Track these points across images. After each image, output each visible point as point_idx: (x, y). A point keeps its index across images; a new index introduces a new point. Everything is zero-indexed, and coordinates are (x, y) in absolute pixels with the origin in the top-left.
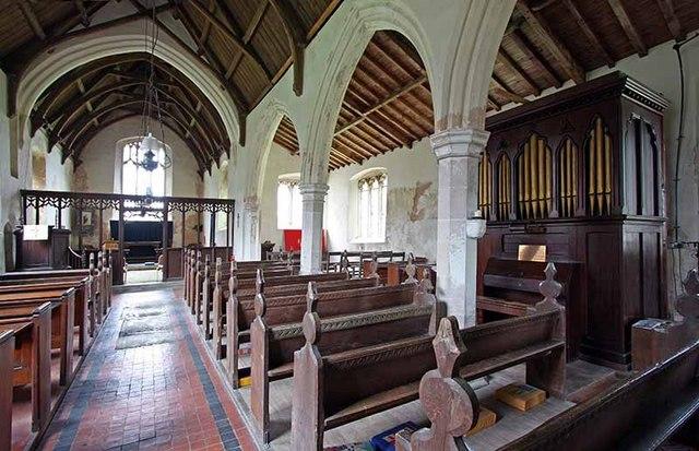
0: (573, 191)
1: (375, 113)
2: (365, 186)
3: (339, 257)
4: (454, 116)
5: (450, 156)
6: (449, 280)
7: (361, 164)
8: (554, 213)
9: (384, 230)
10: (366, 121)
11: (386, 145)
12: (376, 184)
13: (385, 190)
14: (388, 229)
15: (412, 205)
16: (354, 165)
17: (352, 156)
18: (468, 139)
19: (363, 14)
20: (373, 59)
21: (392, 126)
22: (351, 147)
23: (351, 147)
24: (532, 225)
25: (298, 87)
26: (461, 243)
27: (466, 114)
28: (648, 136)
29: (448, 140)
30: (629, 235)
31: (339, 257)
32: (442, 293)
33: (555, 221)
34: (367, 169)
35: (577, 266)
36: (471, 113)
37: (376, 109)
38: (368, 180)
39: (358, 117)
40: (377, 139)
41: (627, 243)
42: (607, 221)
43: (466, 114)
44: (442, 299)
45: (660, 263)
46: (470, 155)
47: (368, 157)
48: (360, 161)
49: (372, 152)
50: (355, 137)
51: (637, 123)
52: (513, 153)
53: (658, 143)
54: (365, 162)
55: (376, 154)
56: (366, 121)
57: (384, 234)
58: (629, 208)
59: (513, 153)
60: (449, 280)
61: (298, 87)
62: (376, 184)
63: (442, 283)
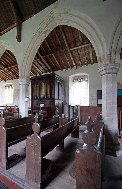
0: (48, 93)
1: (9, 69)
2: (7, 88)
3: (4, 107)
4: (23, 76)
5: (22, 84)
6: (22, 110)
7: (6, 81)
8: (45, 98)
9: (13, 100)
10: (6, 70)
11: (13, 77)
12: (10, 87)
13: (13, 90)
14: (14, 100)
15: (16, 94)
16: (4, 82)
17: (3, 79)
18: (26, 81)
19: (2, 44)
20: (4, 56)
21: (15, 74)
22: (2, 76)
23: (2, 76)
24: (42, 100)
25: (19, 38)
26: (24, 102)
27: (25, 76)
28: (61, 87)
29: (21, 81)
30: (56, 102)
31: (4, 107)
32: (20, 113)
33: (46, 99)
34: (8, 83)
35: (49, 108)
36: (26, 76)
37: (9, 68)
38: (8, 86)
39: (4, 69)
40: (10, 75)
41: (56, 104)
42: (53, 99)
43: (25, 76)
44: (20, 114)
45: (63, 107)
46: (26, 85)
47: (8, 80)
48: (6, 81)
49: (9, 79)
50: (3, 74)
51: (58, 82)
52: (39, 85)
53: (62, 86)
54: (7, 81)
55: (10, 80)
56: (6, 70)
57: (13, 101)
58: (56, 97)
59: (39, 85)
60: (22, 110)
61: (19, 38)
62: (10, 87)
63: (20, 111)
